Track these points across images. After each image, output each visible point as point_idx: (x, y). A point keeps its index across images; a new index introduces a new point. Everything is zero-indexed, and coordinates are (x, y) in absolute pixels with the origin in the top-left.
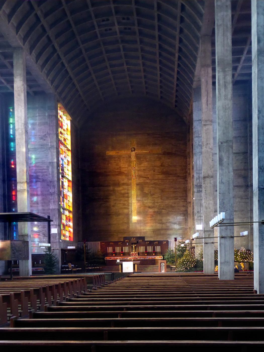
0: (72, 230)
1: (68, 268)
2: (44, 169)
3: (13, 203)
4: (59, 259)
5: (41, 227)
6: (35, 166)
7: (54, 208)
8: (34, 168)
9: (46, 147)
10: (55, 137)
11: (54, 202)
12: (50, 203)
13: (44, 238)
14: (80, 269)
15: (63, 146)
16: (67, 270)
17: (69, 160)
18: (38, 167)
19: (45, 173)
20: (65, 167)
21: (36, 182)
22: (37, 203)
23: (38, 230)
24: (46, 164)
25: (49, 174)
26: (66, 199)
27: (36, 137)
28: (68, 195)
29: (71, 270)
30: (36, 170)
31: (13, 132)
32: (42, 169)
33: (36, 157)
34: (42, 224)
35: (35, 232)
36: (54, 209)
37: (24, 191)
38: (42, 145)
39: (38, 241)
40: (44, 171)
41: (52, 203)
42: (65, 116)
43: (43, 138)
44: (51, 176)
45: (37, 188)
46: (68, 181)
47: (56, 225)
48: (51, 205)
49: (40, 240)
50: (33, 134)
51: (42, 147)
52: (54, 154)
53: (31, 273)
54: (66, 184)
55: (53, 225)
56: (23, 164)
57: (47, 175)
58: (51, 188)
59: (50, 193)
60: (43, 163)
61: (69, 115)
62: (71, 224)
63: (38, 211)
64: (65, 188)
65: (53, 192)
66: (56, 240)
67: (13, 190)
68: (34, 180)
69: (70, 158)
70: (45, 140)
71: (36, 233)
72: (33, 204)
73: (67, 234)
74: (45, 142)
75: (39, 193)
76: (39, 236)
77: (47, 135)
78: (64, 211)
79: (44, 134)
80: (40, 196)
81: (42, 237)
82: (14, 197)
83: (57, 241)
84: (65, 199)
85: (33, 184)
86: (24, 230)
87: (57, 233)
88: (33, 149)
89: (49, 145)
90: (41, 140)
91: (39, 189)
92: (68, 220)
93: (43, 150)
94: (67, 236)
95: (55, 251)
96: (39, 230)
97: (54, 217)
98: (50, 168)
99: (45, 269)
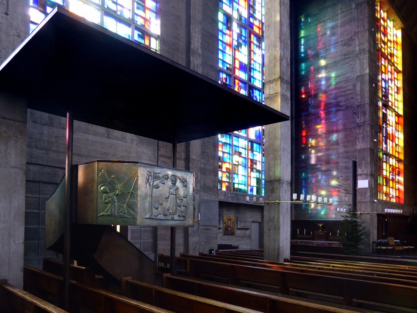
0: (402, 188)
1: (387, 244)
2: (348, 90)
3: (302, 147)
4: (369, 231)
5: (342, 180)
6: (336, 88)
7: (363, 147)
8: (334, 92)
9: (352, 56)
10: (367, 35)
11: (363, 137)
12: (357, 140)
13: (346, 196)
14: (410, 247)
15: (387, 62)
16: (383, 248)
17: (398, 86)
18: (339, 88)
19: (351, 96)
20: (392, 95)
21: (337, 111)
22: (337, 143)
23: (337, 184)
24: (351, 82)
25: (357, 94)
26: (392, 141)
27: (336, 45)
28: (397, 136)
29: (393, 249)
30: (336, 94)
31: (304, 48)
32: (346, 91)
33: (336, 75)
34: (343, 175)
35: (332, 187)
36: (364, 149)
37: (276, 96)
38: (345, 55)
39: (337, 201)
40: (348, 92)
41: (360, 139)
42: (392, 22)
43: (348, 43)
44: (359, 97)
45: (338, 120)
46: (396, 115)
47: (367, 175)
48: (358, 143)
49: (339, 199)
50: (332, 43)
51: (346, 57)
52: (365, 61)
53: (286, 252)
54: (392, 118)
55: (361, 175)
56: (275, 46)
57: (352, 98)
58: (359, 117)
59: (358, 124)
60: (347, 80)
61: (399, 17)
62: (401, 179)
63: (337, 156)
64: (391, 124)
65: (363, 121)
66: (365, 198)
67: (303, 129)
68: (333, 109)
69: (400, 84)
70: (350, 45)
71: (334, 190)
72: (332, 145)
73: (393, 193)
74: (351, 48)
75: (340, 127)
76: (339, 193)
77: (353, 37)
78: (388, 157)
79: (350, 36)
80: (341, 133)
81: (343, 195)
82: (304, 139)
83: (368, 199)
84: (391, 142)
85: (332, 116)
86: (274, 170)
87: (367, 188)
88: (334, 64)
89: (357, 50)
90: (345, 48)
91: (340, 122)
92: (394, 173)
93: (347, 61)
94: (393, 195)
95: (364, 217)
96: (339, 184)
97: (363, 161)
98: (359, 85)
99: (344, 244)
